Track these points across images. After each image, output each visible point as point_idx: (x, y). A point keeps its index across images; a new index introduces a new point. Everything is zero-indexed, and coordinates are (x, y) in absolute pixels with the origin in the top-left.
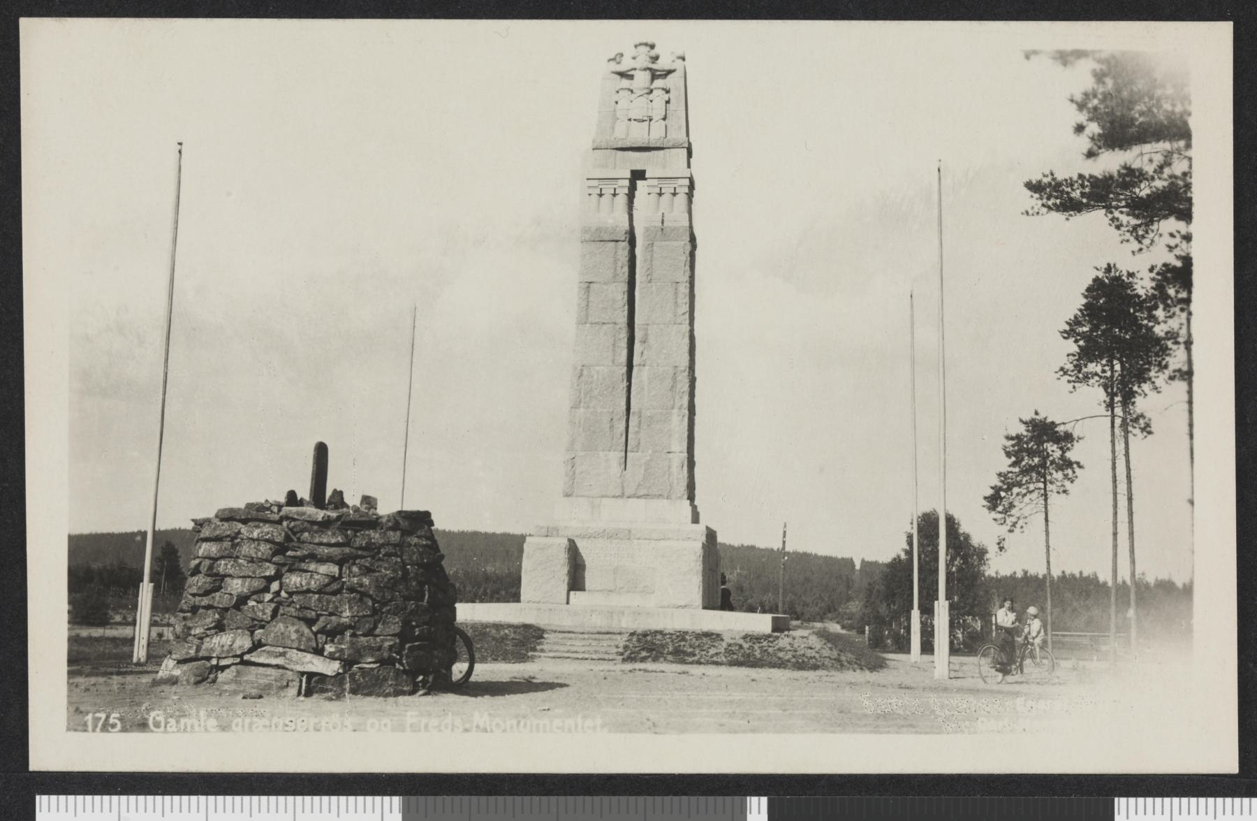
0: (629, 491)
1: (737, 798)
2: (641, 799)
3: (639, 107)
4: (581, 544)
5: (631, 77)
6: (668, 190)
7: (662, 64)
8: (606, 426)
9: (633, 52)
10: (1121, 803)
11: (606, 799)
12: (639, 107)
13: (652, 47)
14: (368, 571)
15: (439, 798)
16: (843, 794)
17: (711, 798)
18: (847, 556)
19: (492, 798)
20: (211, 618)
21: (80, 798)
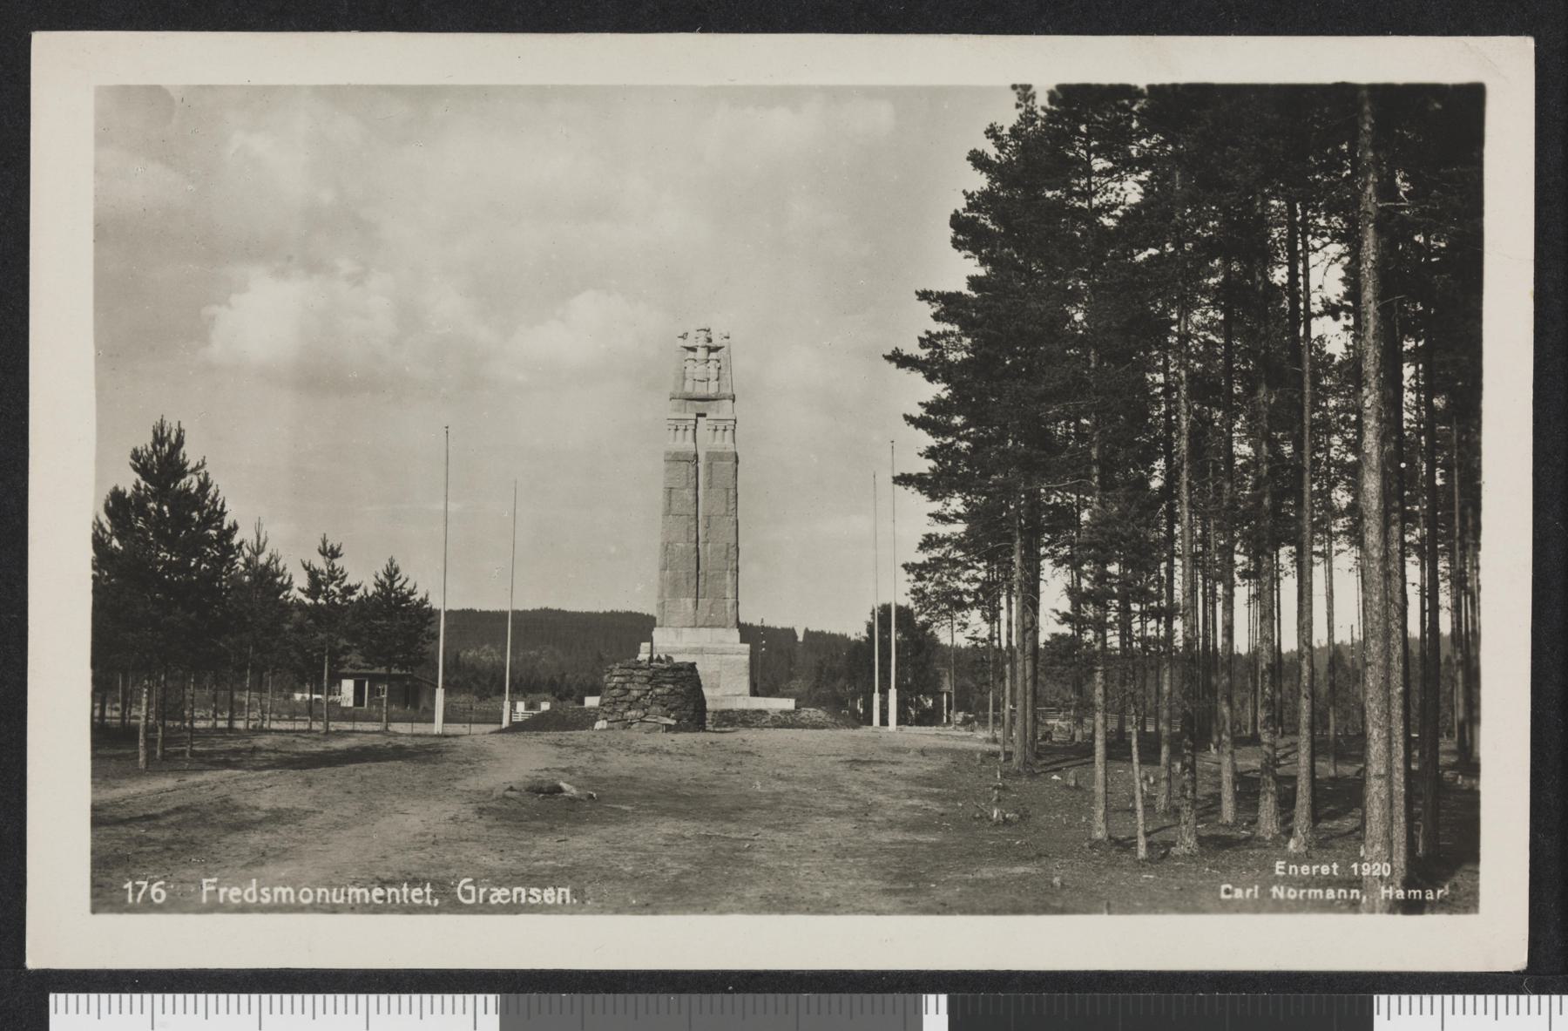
0: (700, 622)
3: (699, 371)
6: (721, 427)
7: (716, 342)
12: (699, 371)
18: (787, 624)
20: (626, 705)
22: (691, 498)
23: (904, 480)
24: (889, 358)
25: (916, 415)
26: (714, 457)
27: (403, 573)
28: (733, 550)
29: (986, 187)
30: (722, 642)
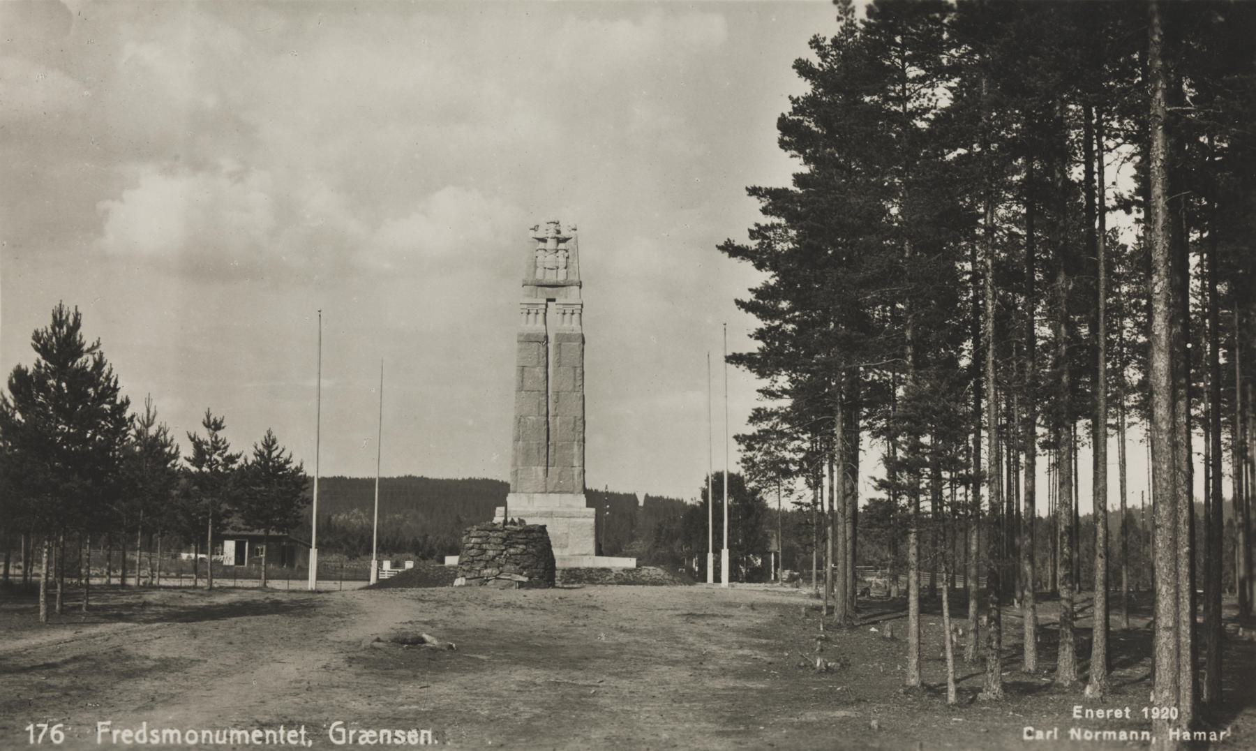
0: (550, 489)
3: (550, 259)
7: (564, 234)
8: (535, 451)
12: (550, 259)
18: (629, 491)
20: (482, 564)
22: (542, 376)
23: (735, 359)
25: (747, 300)
26: (563, 338)
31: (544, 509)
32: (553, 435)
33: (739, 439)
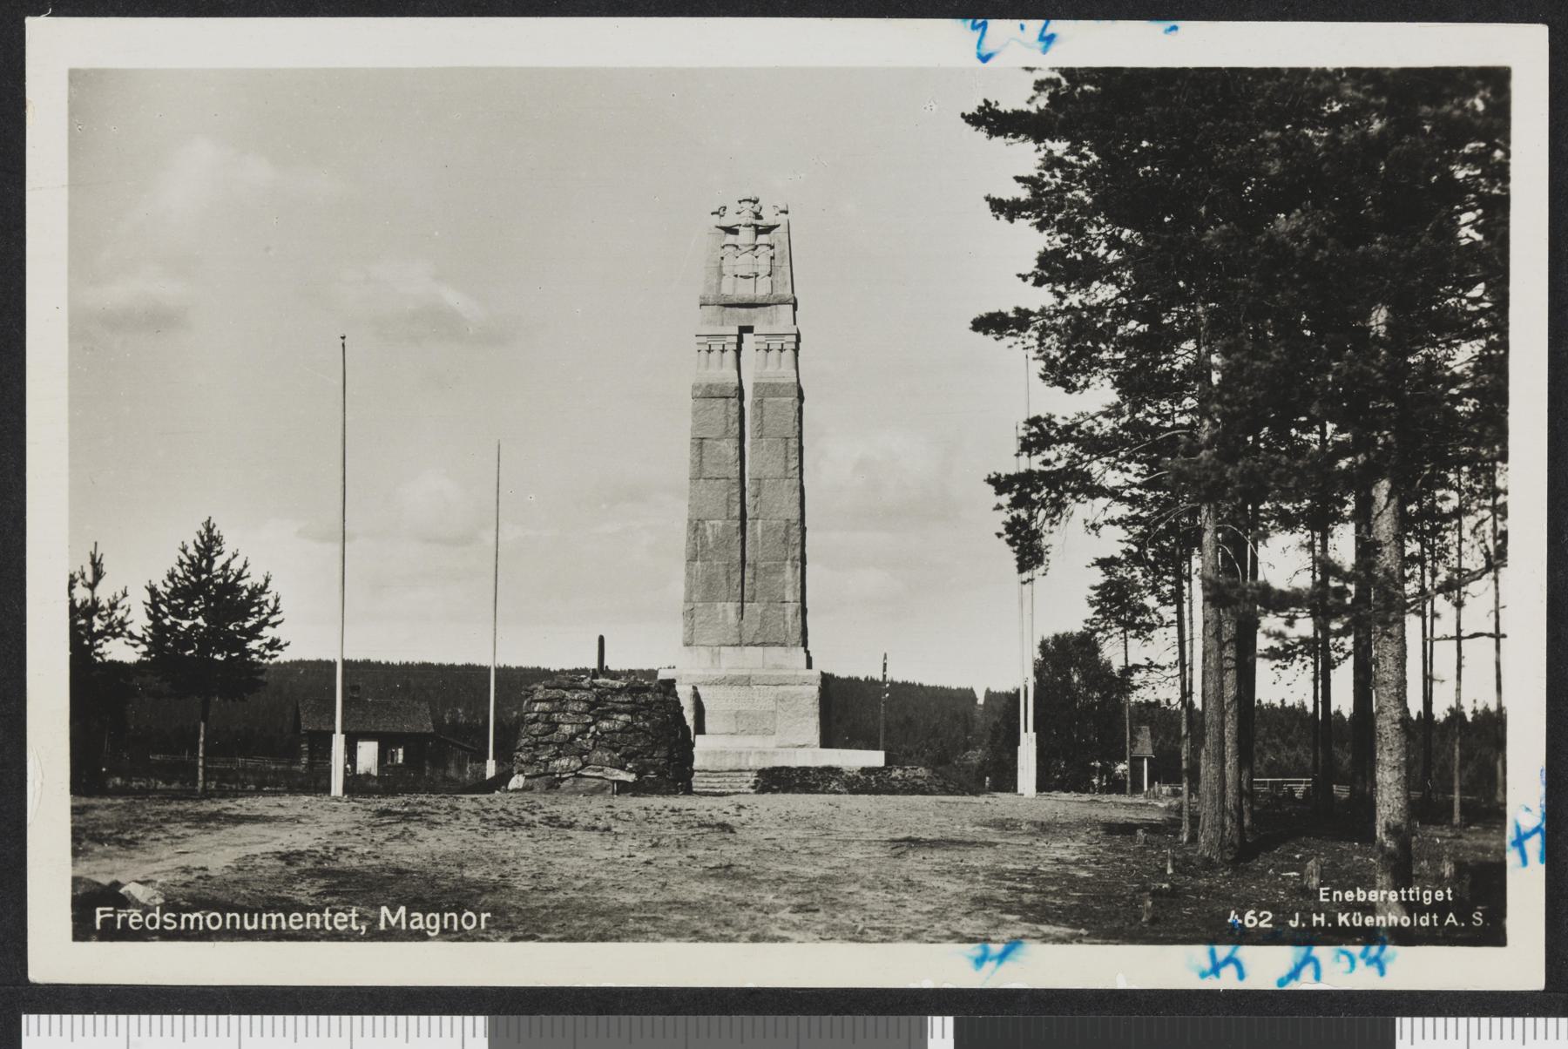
1: (915, 1019)
2: (792, 1019)
3: (744, 263)
4: (700, 690)
5: (736, 232)
6: (776, 345)
7: (768, 219)
9: (738, 207)
10: (1404, 1024)
11: (748, 1019)
12: (744, 263)
13: (756, 202)
14: (647, 718)
15: (535, 1018)
16: (1050, 1013)
17: (882, 1019)
18: (965, 685)
19: (603, 1018)
21: (78, 1018)
22: (733, 453)
23: (993, 324)
24: (974, 120)
25: (1007, 196)
26: (767, 390)
27: (228, 548)
28: (795, 531)
29: (1270, 615)
30: (777, 667)
31: (736, 673)
32: (751, 553)
33: (1000, 484)
